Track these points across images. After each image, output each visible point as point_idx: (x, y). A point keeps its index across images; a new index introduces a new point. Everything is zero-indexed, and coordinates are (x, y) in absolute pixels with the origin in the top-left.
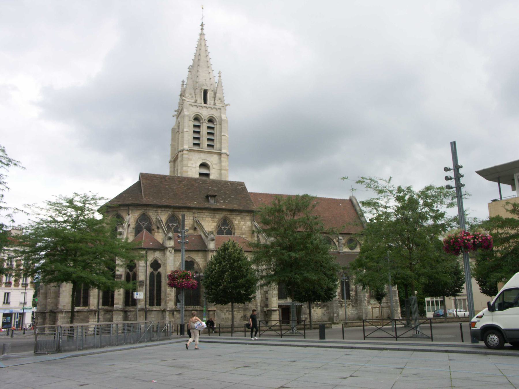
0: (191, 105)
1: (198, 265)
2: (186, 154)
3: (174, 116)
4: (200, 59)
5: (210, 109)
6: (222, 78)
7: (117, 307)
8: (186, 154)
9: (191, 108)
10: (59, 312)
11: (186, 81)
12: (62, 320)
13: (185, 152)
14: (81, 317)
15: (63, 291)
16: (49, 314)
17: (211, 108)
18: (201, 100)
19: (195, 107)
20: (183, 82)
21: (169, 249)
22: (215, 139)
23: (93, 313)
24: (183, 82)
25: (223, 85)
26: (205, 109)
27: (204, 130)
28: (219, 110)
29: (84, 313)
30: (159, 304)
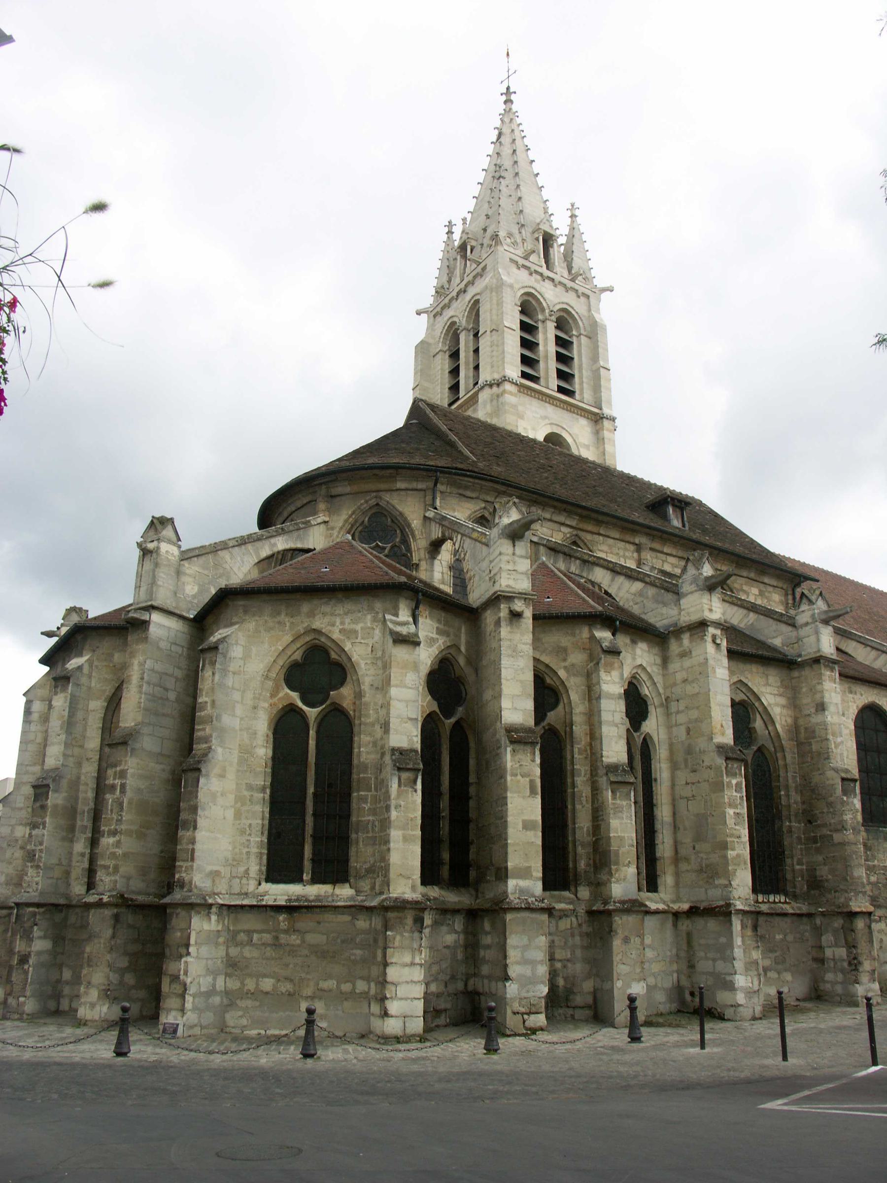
0: (516, 263)
1: (769, 720)
2: (511, 393)
3: (419, 313)
4: (507, 168)
5: (560, 289)
6: (579, 220)
7: (522, 891)
8: (511, 393)
9: (514, 269)
10: (190, 907)
11: (469, 217)
12: (204, 951)
13: (508, 386)
14: (313, 938)
15: (214, 796)
16: (108, 912)
17: (565, 285)
18: (537, 260)
19: (524, 273)
20: (450, 225)
21: (711, 630)
22: (576, 373)
23: (409, 921)
24: (450, 225)
25: (584, 238)
26: (548, 284)
27: (547, 346)
28: (582, 299)
29: (328, 916)
30: (333, 869)
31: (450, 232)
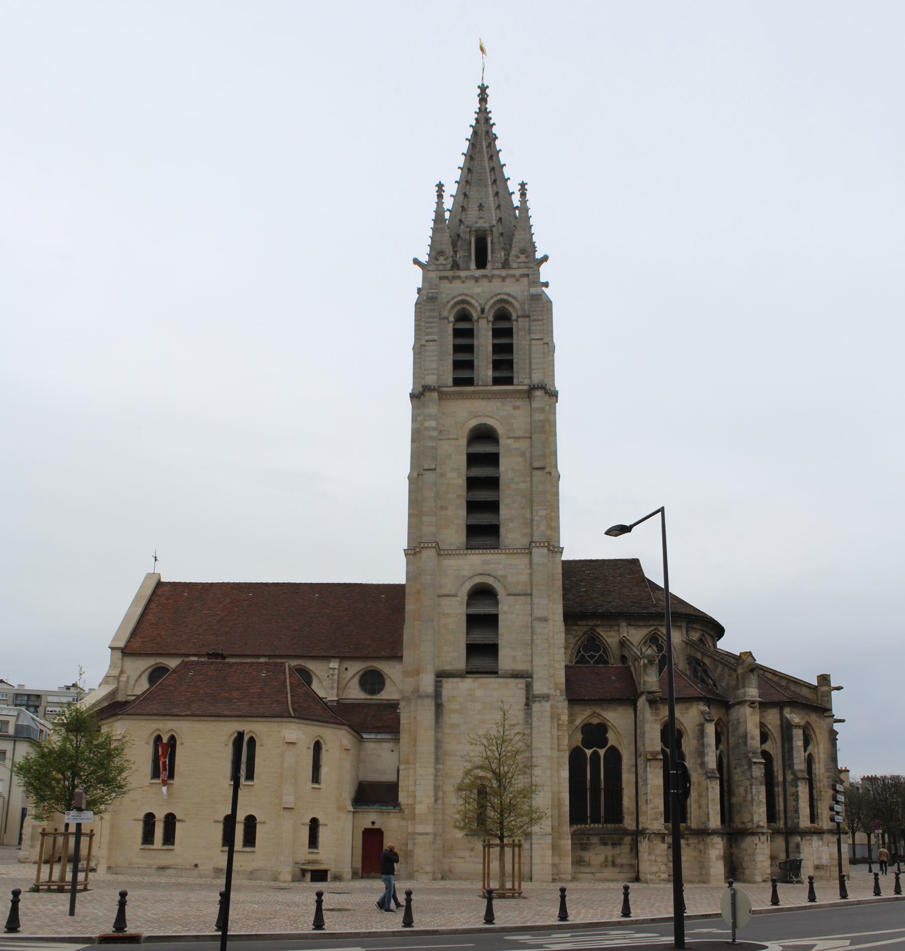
20: (440, 186)
24: (440, 186)
31: (440, 196)
